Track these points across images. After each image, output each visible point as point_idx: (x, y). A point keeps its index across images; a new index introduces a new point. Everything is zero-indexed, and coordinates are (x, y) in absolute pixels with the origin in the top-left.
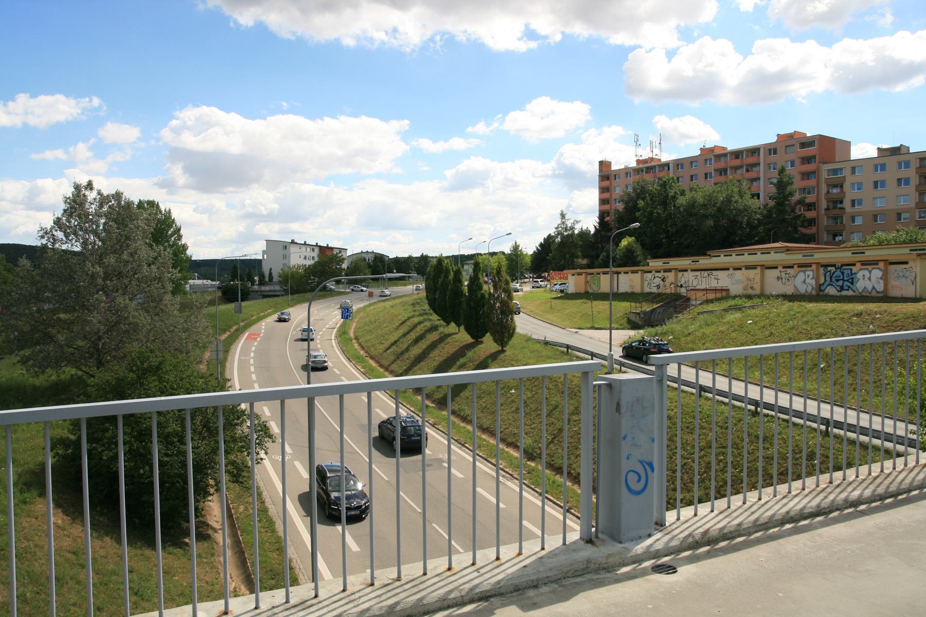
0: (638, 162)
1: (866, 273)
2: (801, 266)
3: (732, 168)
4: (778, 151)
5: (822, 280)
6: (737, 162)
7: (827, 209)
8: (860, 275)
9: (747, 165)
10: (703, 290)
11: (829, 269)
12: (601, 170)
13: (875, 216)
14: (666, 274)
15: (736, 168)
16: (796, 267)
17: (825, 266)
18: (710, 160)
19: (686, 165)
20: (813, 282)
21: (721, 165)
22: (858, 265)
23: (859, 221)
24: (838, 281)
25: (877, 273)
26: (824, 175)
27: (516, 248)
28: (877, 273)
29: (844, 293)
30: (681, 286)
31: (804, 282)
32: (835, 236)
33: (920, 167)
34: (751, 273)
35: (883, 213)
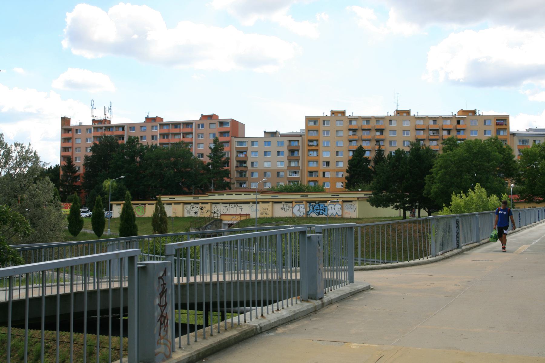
0: (94, 121)
1: (333, 206)
2: (296, 202)
3: (172, 134)
4: (205, 126)
5: (308, 210)
6: (176, 131)
7: (237, 167)
8: (329, 207)
9: (183, 133)
10: (239, 215)
11: (312, 204)
12: (63, 125)
14: (204, 205)
15: (175, 134)
16: (294, 202)
17: (310, 202)
18: (156, 126)
19: (137, 128)
20: (304, 211)
21: (165, 130)
23: (256, 176)
24: (317, 210)
25: (338, 206)
26: (235, 145)
28: (338, 206)
29: (320, 216)
30: (215, 213)
31: (299, 210)
33: (289, 146)
34: (266, 205)
35: (270, 171)
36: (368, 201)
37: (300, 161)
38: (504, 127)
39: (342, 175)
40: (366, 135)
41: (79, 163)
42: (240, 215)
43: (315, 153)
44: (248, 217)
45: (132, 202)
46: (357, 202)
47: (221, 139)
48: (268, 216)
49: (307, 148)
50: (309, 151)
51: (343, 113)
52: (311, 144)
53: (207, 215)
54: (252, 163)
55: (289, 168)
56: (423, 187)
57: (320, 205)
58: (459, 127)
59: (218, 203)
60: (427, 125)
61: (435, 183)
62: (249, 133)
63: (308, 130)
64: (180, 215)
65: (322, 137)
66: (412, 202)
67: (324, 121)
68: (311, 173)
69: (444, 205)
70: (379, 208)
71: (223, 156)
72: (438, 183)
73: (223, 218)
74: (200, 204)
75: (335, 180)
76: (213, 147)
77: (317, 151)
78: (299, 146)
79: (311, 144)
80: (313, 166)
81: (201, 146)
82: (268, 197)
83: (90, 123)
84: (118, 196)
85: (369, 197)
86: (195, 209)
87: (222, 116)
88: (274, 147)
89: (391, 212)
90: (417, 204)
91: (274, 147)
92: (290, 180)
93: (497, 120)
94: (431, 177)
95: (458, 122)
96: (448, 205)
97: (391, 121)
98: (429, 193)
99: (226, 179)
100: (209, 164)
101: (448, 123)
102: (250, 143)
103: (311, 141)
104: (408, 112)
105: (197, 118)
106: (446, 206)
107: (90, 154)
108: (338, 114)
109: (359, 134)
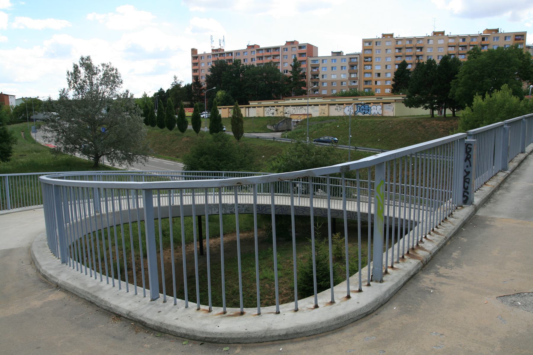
0: (213, 50)
1: (375, 107)
2: (347, 104)
3: (265, 56)
4: (288, 49)
5: (356, 110)
7: (311, 79)
8: (372, 108)
12: (192, 54)
13: (332, 83)
14: (278, 108)
17: (357, 104)
18: (254, 51)
19: (241, 53)
21: (260, 54)
22: (372, 104)
23: (325, 85)
26: (310, 63)
27: (145, 95)
28: (379, 107)
29: (365, 115)
32: (315, 92)
34: (324, 107)
35: (336, 81)
36: (403, 102)
37: (358, 74)
38: (521, 41)
39: (389, 83)
40: (409, 52)
41: (203, 80)
42: (304, 115)
43: (370, 66)
44: (310, 116)
45: (218, 107)
46: (394, 104)
47: (299, 59)
48: (325, 115)
49: (363, 63)
50: (365, 65)
51: (392, 35)
52: (366, 60)
53: (280, 115)
54: (323, 75)
55: (350, 79)
56: (448, 91)
57: (366, 106)
58: (483, 43)
59: (289, 106)
60: (457, 42)
61: (459, 87)
62: (322, 53)
63: (364, 49)
64: (261, 115)
65: (375, 54)
66: (440, 103)
67: (376, 42)
68: (366, 82)
69: (466, 105)
70: (412, 108)
71: (300, 71)
72: (461, 86)
73: (293, 117)
74: (276, 107)
75: (383, 88)
76: (293, 65)
77: (371, 65)
78: (357, 62)
79: (366, 60)
80: (368, 76)
81: (286, 64)
82: (329, 101)
83: (210, 52)
84: (225, 102)
85: (404, 100)
86: (272, 111)
87: (301, 42)
88: (339, 63)
89: (422, 111)
90: (444, 105)
91: (339, 63)
92: (351, 88)
93: (516, 36)
94: (456, 82)
95: (483, 39)
96: (470, 104)
97: (428, 40)
98: (453, 96)
99: (304, 88)
100: (290, 77)
101: (475, 40)
102: (321, 61)
103: (367, 58)
104: (443, 33)
105: (283, 44)
106: (468, 106)
107: (209, 73)
108: (388, 36)
109: (403, 51)
